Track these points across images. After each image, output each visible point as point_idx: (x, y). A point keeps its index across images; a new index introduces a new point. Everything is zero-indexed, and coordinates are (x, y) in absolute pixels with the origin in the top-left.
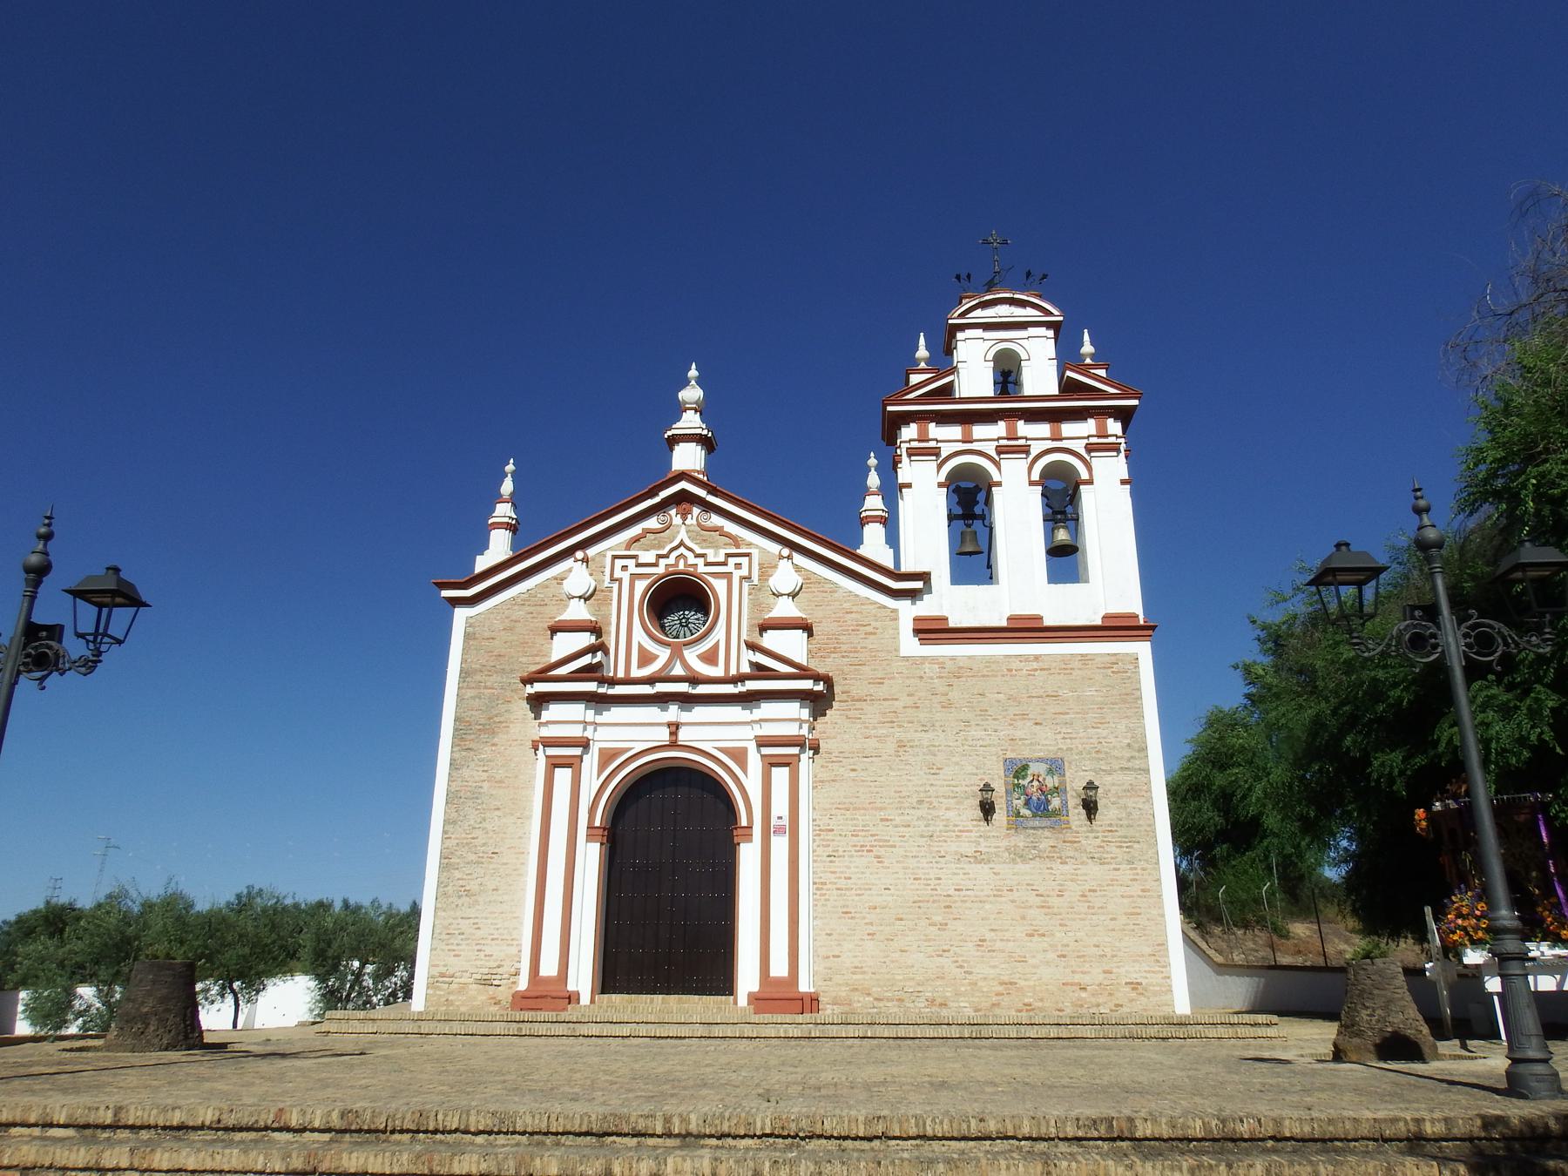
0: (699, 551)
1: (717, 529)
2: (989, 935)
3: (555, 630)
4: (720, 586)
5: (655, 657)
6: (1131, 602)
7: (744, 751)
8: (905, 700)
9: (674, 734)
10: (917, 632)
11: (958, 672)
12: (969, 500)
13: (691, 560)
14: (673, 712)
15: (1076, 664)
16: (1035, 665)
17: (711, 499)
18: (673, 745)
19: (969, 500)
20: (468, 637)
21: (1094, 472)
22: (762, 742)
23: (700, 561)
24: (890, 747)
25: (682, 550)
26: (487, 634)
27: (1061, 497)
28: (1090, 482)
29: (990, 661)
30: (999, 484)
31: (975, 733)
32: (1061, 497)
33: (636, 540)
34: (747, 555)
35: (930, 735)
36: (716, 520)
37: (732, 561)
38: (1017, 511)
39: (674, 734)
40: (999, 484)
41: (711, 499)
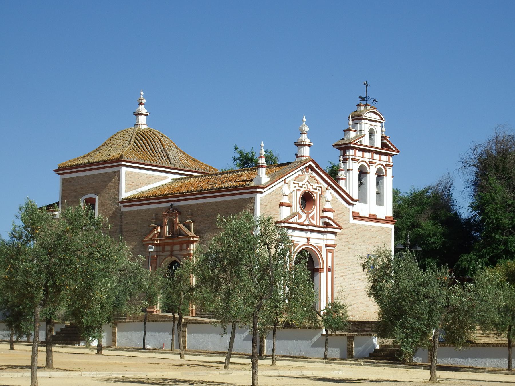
0: (312, 184)
1: (314, 177)
2: (363, 300)
3: (281, 205)
4: (315, 195)
5: (126, 191)
6: (390, 214)
7: (321, 248)
8: (350, 236)
9: (308, 240)
10: (353, 216)
11: (360, 229)
12: (362, 173)
13: (309, 187)
14: (309, 234)
15: (381, 229)
16: (374, 229)
17: (316, 168)
18: (308, 244)
19: (362, 173)
20: (261, 204)
21: (387, 173)
22: (327, 245)
23: (311, 187)
24: (347, 249)
25: (320, 189)
26: (265, 204)
27: (380, 176)
28: (386, 176)
29: (366, 226)
30: (369, 173)
31: (362, 246)
32: (380, 176)
33: (297, 177)
34: (321, 187)
35: (354, 246)
36: (314, 174)
37: (318, 188)
38: (371, 178)
39: (308, 240)
40: (369, 173)
41: (316, 168)
